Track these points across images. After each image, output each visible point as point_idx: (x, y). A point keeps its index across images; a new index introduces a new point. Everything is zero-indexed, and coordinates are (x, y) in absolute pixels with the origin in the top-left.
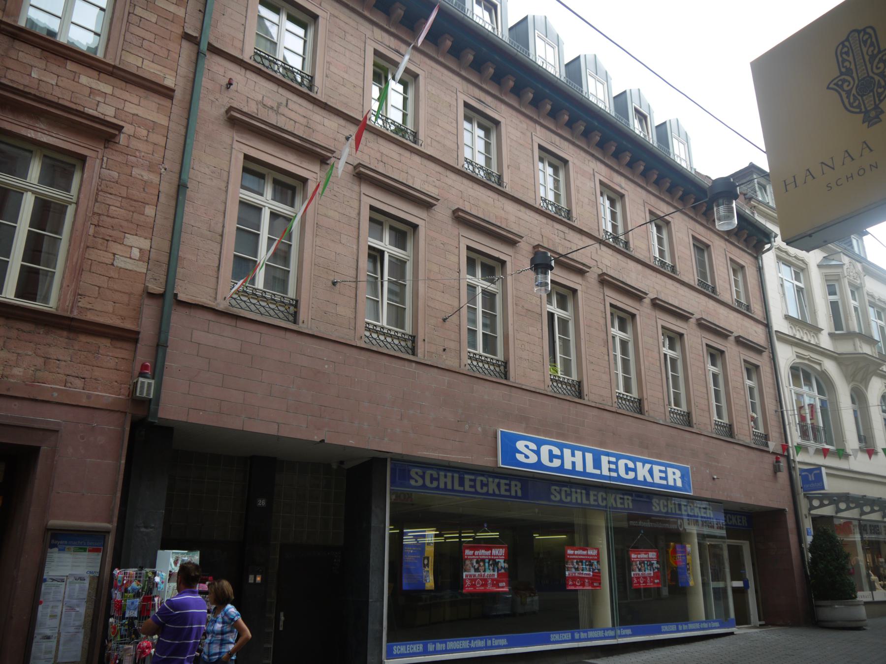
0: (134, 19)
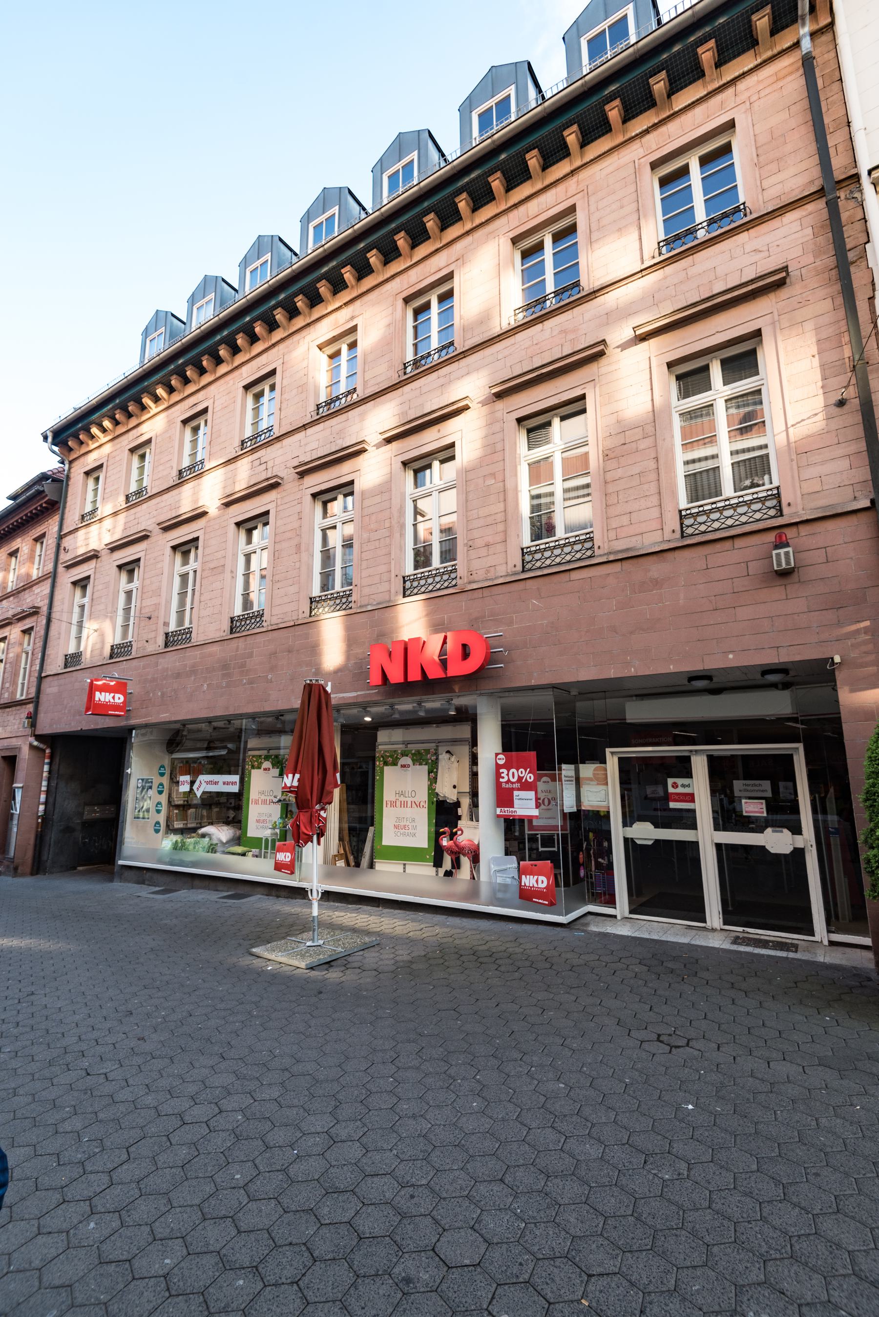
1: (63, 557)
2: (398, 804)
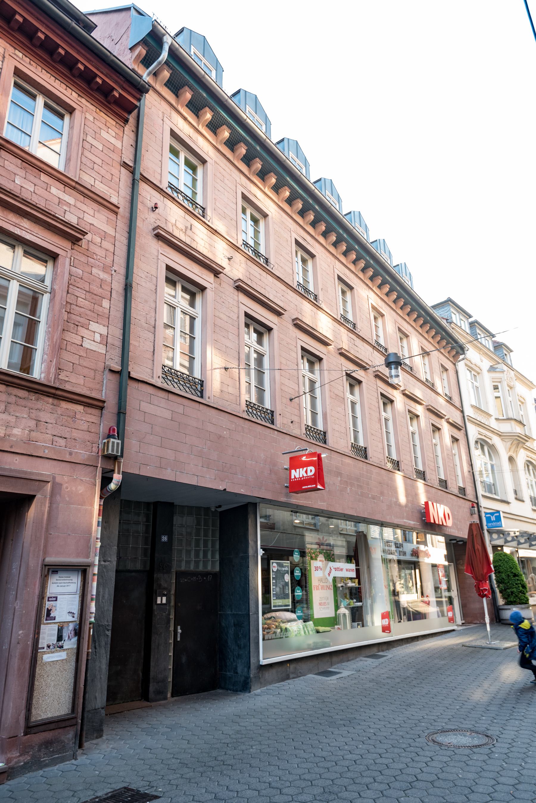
0: (87, 146)
2: (320, 587)
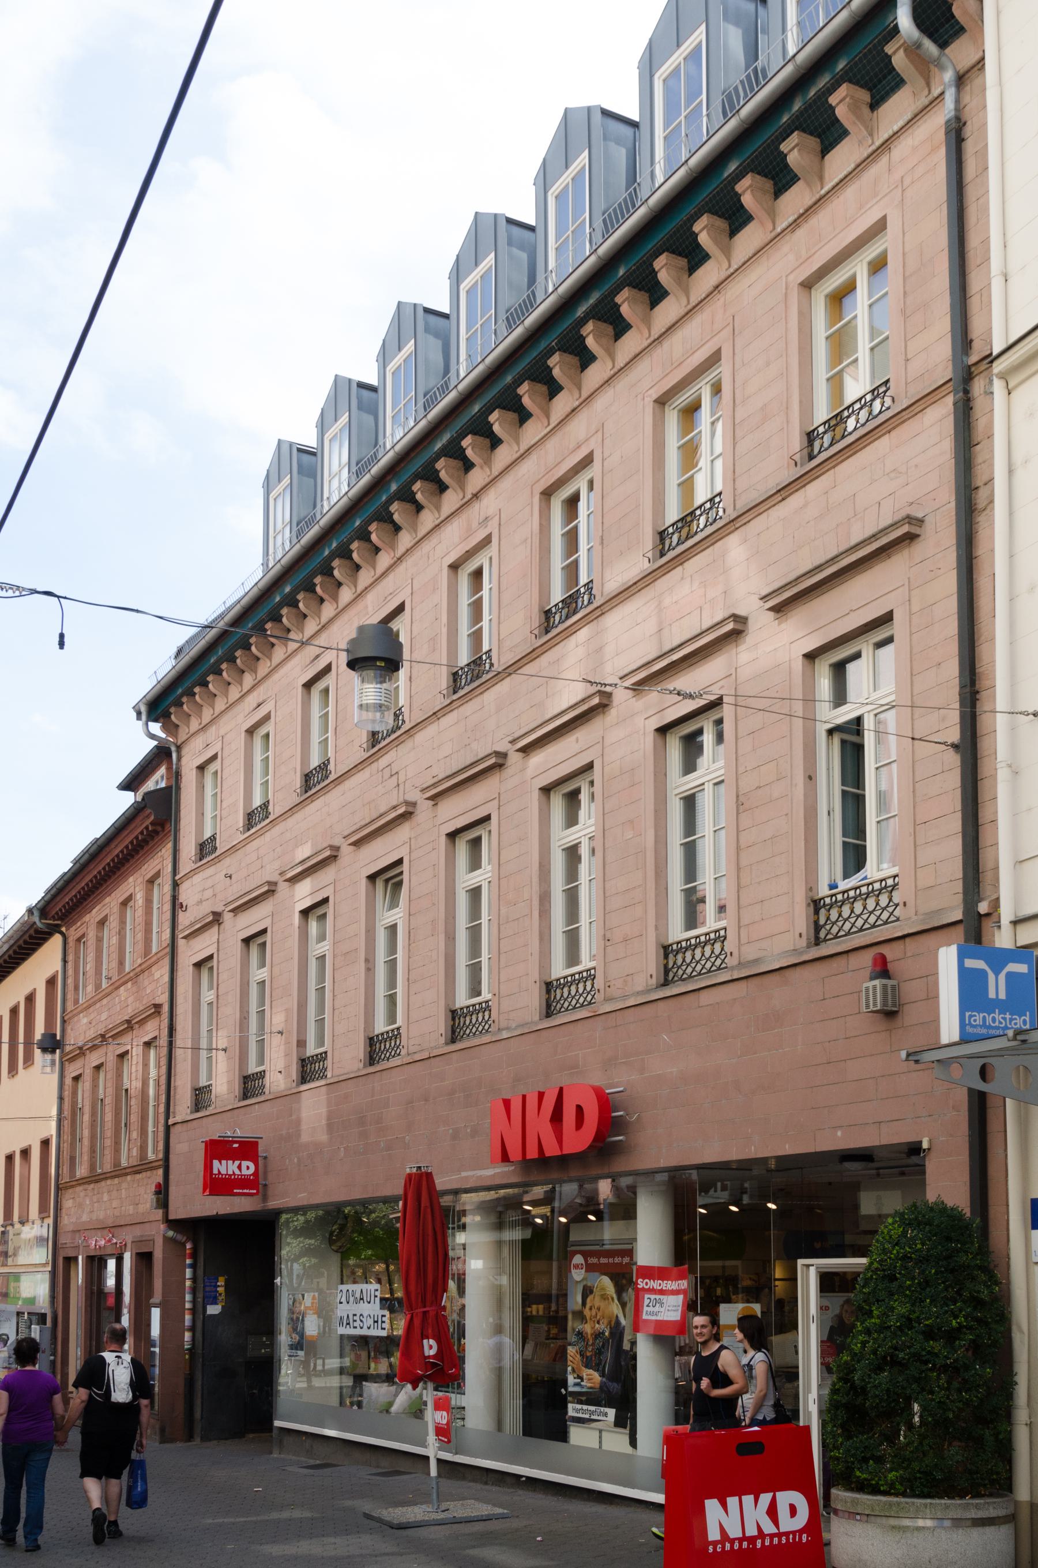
1: (184, 919)
